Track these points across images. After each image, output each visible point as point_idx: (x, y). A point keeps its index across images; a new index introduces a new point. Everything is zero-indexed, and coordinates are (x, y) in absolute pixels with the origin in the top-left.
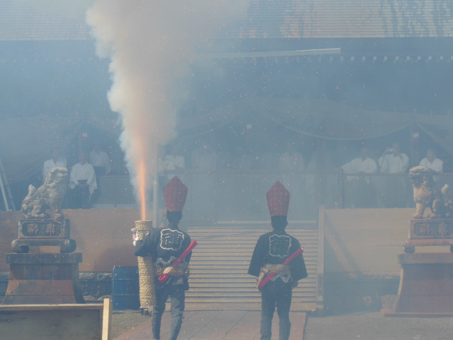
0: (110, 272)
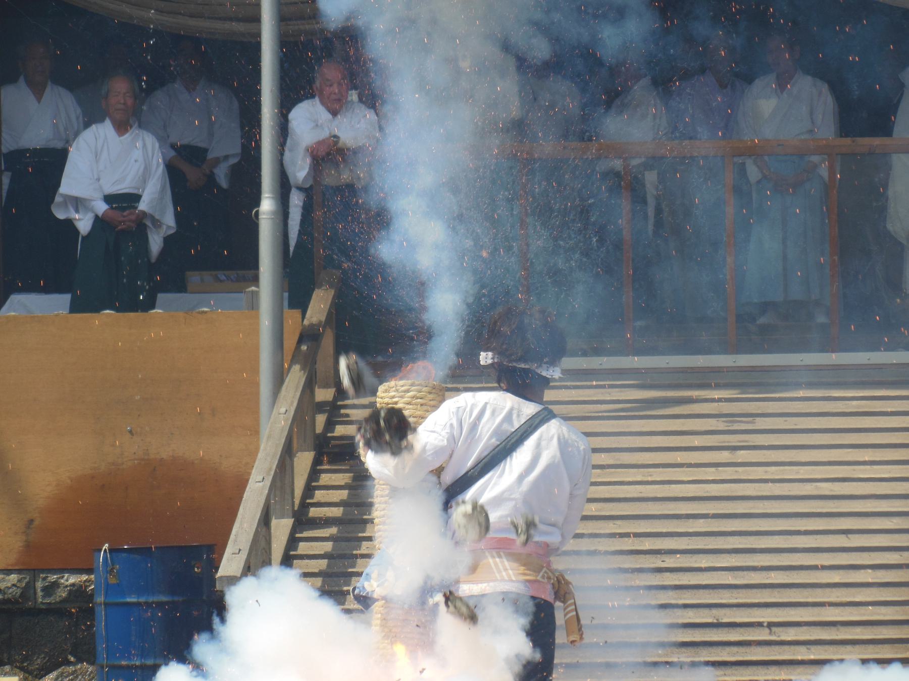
0: (89, 571)
